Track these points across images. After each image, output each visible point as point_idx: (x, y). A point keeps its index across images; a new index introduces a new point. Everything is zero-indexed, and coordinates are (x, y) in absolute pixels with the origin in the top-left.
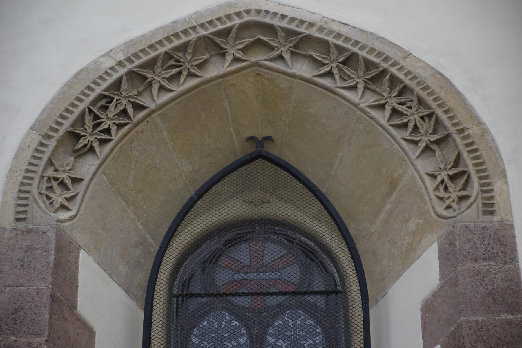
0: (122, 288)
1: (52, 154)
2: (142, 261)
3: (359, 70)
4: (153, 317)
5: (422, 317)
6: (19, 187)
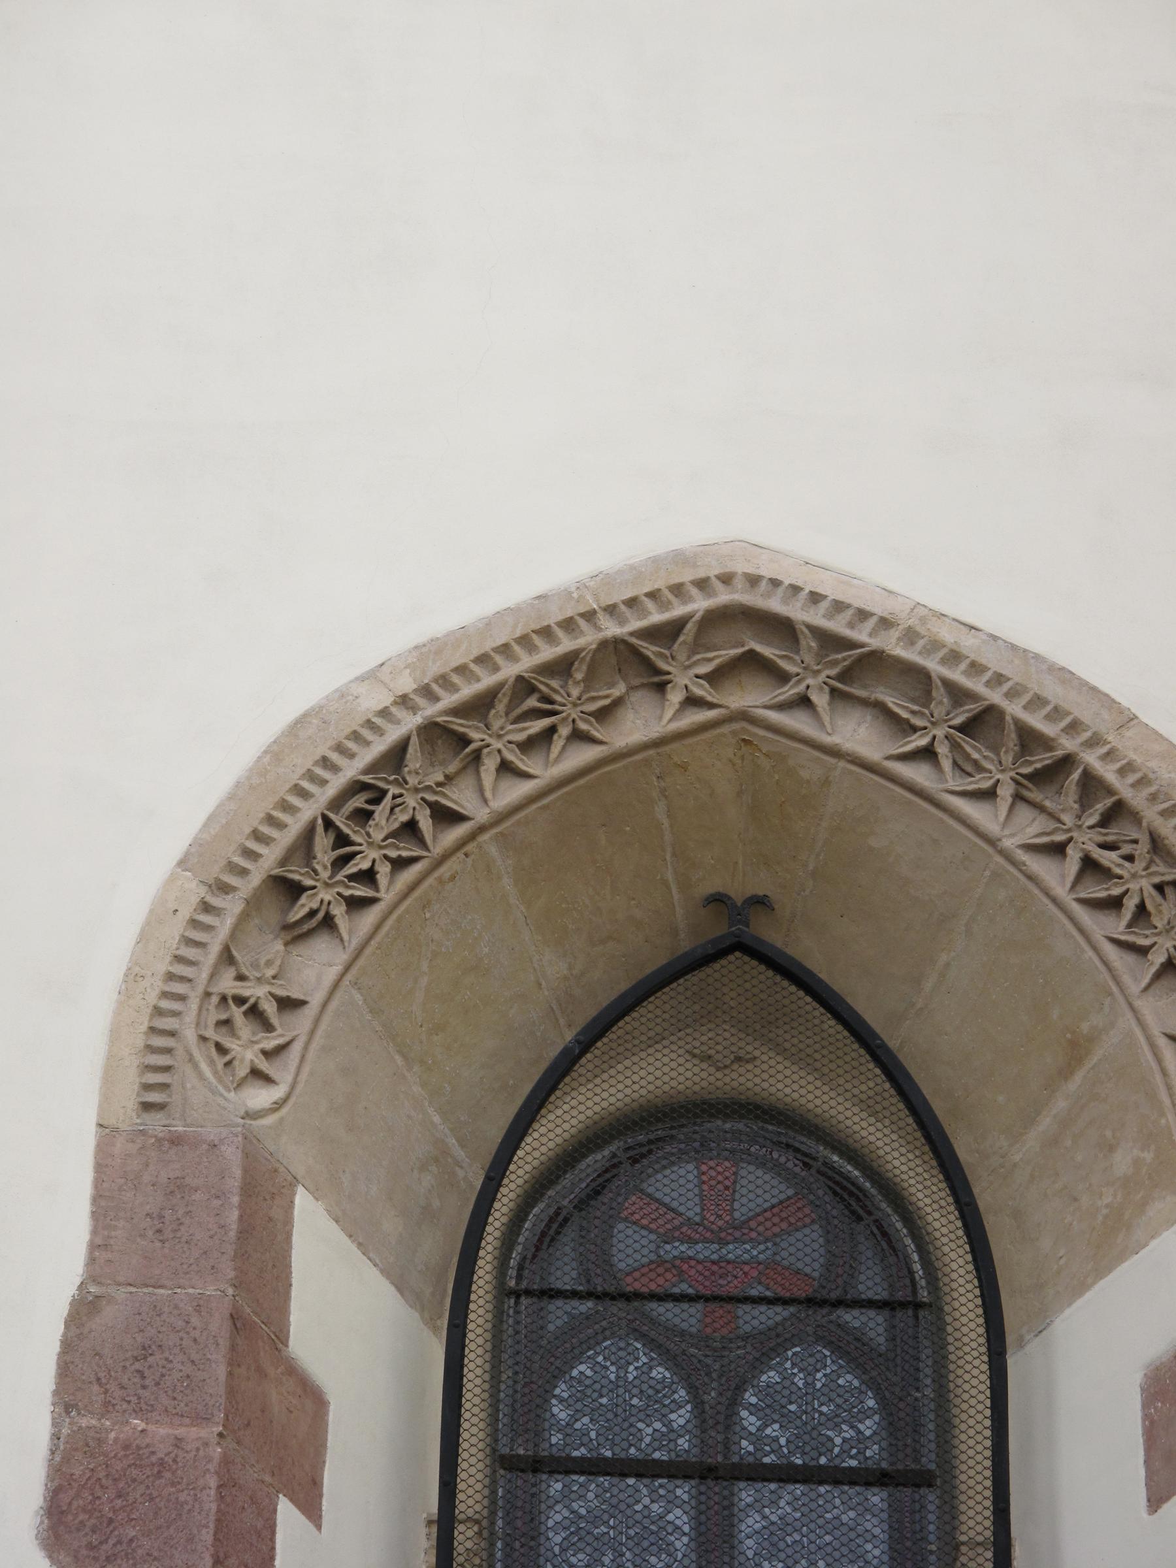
0: (388, 1278)
1: (233, 934)
2: (436, 1203)
3: (1004, 750)
4: (466, 1361)
5: (1145, 1405)
6: (150, 1020)
